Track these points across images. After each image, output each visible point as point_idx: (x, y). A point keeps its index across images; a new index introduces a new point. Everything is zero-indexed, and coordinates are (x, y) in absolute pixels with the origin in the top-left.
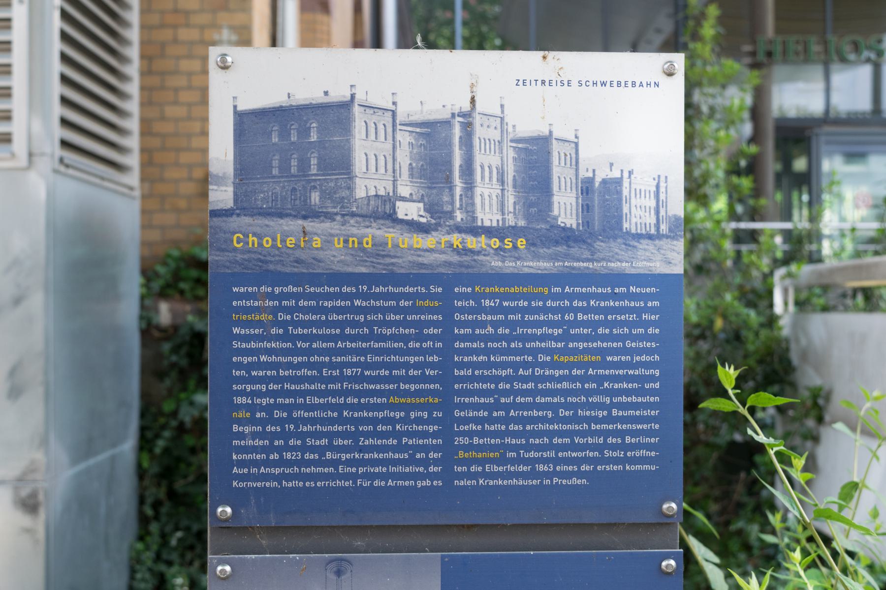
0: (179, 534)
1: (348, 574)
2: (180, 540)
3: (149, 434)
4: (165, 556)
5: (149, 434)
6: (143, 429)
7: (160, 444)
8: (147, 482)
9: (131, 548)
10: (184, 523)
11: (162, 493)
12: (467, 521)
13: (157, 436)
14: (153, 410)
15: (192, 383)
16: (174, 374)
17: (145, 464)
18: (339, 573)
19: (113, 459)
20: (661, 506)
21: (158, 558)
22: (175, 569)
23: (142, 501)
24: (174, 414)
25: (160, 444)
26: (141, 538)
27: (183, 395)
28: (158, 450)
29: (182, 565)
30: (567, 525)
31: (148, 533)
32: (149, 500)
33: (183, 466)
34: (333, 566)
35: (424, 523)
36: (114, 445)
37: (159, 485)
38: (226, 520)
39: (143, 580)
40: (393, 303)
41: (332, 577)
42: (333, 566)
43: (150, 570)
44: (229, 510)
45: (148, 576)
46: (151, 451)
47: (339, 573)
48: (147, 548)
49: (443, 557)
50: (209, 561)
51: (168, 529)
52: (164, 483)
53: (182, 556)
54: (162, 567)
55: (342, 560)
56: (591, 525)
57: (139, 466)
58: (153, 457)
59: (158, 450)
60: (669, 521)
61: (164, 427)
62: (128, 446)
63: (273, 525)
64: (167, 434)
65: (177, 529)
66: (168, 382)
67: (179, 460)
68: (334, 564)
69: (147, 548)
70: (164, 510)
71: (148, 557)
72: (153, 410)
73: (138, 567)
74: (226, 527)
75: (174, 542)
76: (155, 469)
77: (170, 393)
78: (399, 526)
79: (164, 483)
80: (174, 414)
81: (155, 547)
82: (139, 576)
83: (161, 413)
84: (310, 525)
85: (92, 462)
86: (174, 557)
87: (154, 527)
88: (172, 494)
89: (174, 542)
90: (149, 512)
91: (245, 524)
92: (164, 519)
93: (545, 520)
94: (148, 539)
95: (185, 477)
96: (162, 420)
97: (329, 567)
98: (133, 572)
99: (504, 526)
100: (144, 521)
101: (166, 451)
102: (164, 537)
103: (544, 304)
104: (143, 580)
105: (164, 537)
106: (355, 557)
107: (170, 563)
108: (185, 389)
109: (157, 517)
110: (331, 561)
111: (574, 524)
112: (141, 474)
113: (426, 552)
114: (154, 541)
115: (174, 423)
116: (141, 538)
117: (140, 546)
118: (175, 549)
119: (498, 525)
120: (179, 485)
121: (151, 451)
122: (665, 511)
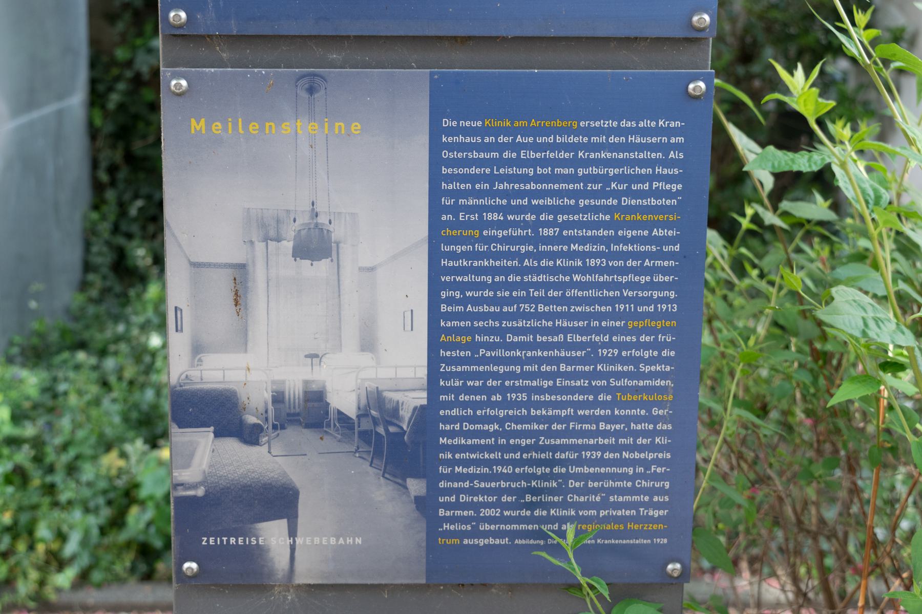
0: (139, 203)
1: (322, 92)
2: (141, 209)
3: (101, 88)
4: (124, 227)
5: (101, 88)
6: (93, 82)
7: (114, 99)
8: (100, 143)
9: (85, 218)
10: (144, 190)
11: (118, 156)
12: (461, 32)
13: (110, 89)
14: (105, 59)
15: (149, 28)
16: (127, 16)
17: (98, 122)
18: (311, 90)
19: (60, 113)
20: (691, 18)
21: (116, 230)
22: (135, 243)
23: (95, 164)
24: (129, 63)
25: (114, 99)
26: (96, 207)
27: (139, 42)
28: (111, 106)
29: (144, 238)
30: (578, 39)
31: (104, 201)
32: (104, 164)
33: (141, 125)
34: (304, 83)
35: (411, 34)
36: (61, 97)
37: (113, 147)
38: (180, 27)
39: (100, 254)
40: (467, 484)
41: (304, 95)
42: (304, 83)
43: (108, 243)
44: (183, 15)
45: (105, 249)
46: (103, 107)
47: (311, 90)
48: (104, 218)
49: (432, 74)
50: (161, 74)
51: (127, 196)
52: (121, 145)
53: (144, 228)
54: (120, 240)
55: (315, 75)
56: (606, 40)
57: (91, 125)
58: (106, 114)
59: (111, 106)
60: (699, 35)
61: (117, 79)
62: (77, 99)
63: (235, 33)
64: (121, 86)
65: (136, 197)
66: (120, 26)
67: (136, 117)
68: (306, 80)
69: (104, 218)
70: (122, 175)
71: (105, 228)
72: (105, 59)
73: (94, 239)
74: (180, 36)
75: (133, 211)
76: (109, 128)
77: (124, 40)
78: (381, 37)
79: (121, 145)
80: (129, 63)
81: (112, 217)
82: (95, 249)
83: (113, 62)
84: (277, 34)
85: (35, 115)
86: (135, 228)
87: (110, 195)
88: (130, 158)
89: (133, 211)
90: (104, 177)
91: (202, 31)
92: (121, 186)
93: (552, 33)
94: (105, 208)
95: (144, 137)
96: (115, 71)
97: (300, 83)
98: (87, 245)
99: (504, 39)
100: (98, 188)
101: (121, 107)
102: (122, 207)
103: (655, 427)
104: (100, 254)
105: (122, 207)
106: (330, 72)
107: (129, 236)
108: (140, 34)
109: (113, 183)
110: (303, 76)
111: (587, 38)
112: (93, 133)
113: (412, 68)
114: (111, 210)
115: (129, 74)
116: (96, 207)
117: (95, 216)
118: (135, 220)
119: (498, 37)
120: (138, 146)
121: (103, 107)
122: (697, 25)
